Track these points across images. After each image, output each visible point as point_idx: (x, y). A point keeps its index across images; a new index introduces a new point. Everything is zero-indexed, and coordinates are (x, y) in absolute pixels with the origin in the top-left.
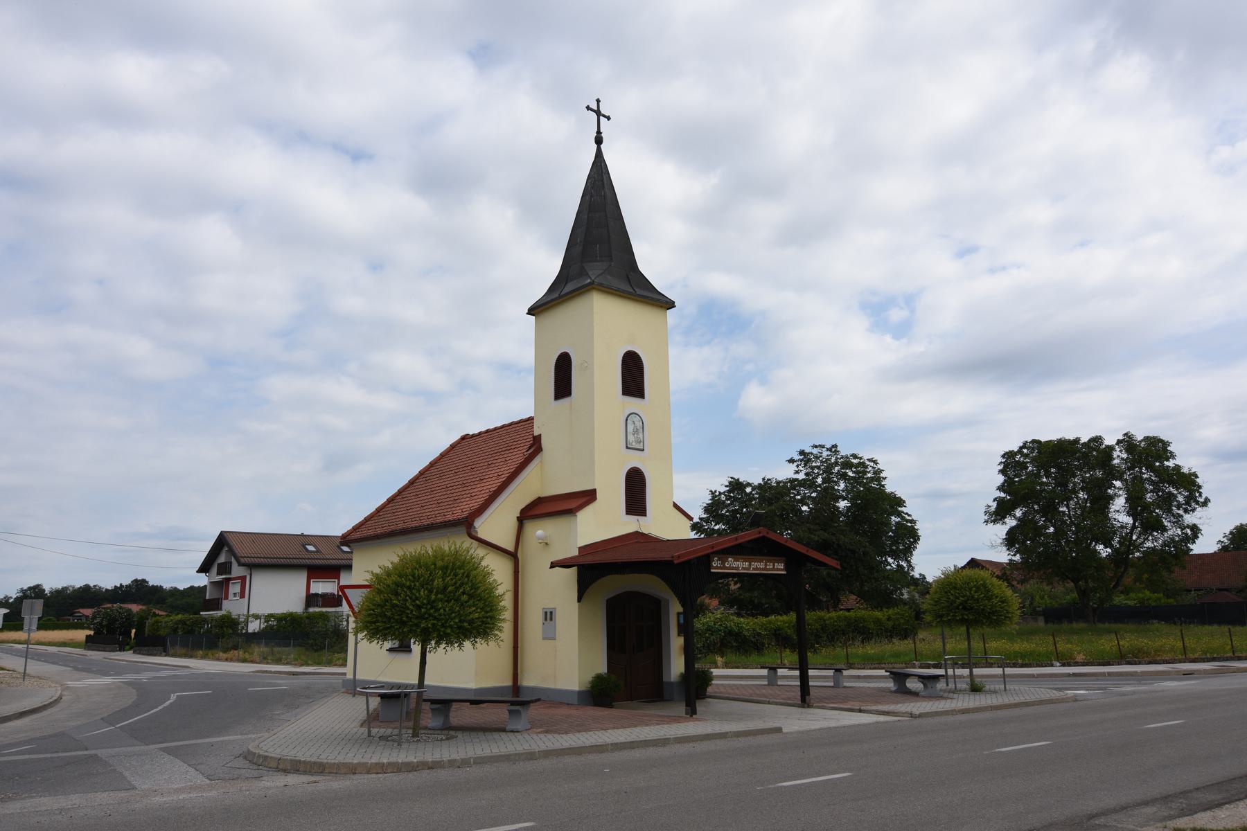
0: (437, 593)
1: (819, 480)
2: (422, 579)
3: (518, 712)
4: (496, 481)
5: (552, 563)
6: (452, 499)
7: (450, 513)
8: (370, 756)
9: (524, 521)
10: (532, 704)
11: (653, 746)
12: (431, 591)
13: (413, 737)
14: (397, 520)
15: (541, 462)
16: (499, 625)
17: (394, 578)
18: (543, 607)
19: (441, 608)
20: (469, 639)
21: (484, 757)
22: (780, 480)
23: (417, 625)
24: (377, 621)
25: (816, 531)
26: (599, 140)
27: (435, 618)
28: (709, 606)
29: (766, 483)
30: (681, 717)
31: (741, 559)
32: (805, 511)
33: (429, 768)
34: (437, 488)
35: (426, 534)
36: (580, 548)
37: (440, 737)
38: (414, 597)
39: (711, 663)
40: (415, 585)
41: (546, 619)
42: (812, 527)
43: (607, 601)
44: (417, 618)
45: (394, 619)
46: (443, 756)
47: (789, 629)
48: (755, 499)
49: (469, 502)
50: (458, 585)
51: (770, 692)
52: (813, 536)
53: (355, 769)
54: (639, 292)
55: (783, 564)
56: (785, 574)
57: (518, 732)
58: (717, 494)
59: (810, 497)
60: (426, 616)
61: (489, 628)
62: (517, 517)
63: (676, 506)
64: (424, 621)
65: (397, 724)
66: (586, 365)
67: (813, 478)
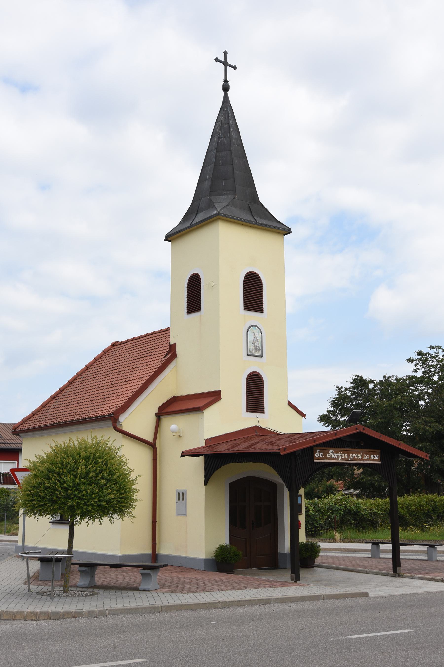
0: (81, 478)
1: (436, 378)
2: (68, 467)
3: (149, 575)
4: (138, 383)
5: (182, 452)
6: (102, 397)
7: (100, 409)
8: (27, 607)
9: (162, 417)
10: (160, 569)
11: (257, 605)
12: (76, 476)
13: (63, 593)
14: (52, 415)
15: (176, 366)
16: (133, 504)
17: (47, 465)
18: (176, 489)
19: (83, 490)
20: (106, 515)
21: (117, 610)
22: (401, 377)
23: (65, 504)
24: (33, 500)
25: (431, 423)
26: (226, 88)
27: (79, 498)
28: (338, 487)
29: (387, 380)
30: (286, 582)
31: (341, 451)
32: (422, 405)
33: (72, 617)
34: (91, 388)
35: (81, 426)
36: (207, 440)
37: (85, 593)
38: (62, 481)
39: (330, 538)
40: (63, 471)
41: (179, 499)
42: (427, 419)
43: (229, 484)
44: (65, 497)
45: (47, 498)
46: (84, 608)
47: (403, 510)
48: (377, 394)
49: (116, 401)
50: (98, 471)
51: (377, 564)
52: (428, 428)
53: (15, 617)
54: (259, 220)
55: (378, 455)
56: (380, 464)
57: (149, 591)
58: (343, 389)
59: (427, 392)
60: (72, 496)
61: (123, 507)
62: (156, 414)
63: (290, 404)
64: (70, 501)
65: (50, 584)
66: (213, 284)
67: (430, 376)
